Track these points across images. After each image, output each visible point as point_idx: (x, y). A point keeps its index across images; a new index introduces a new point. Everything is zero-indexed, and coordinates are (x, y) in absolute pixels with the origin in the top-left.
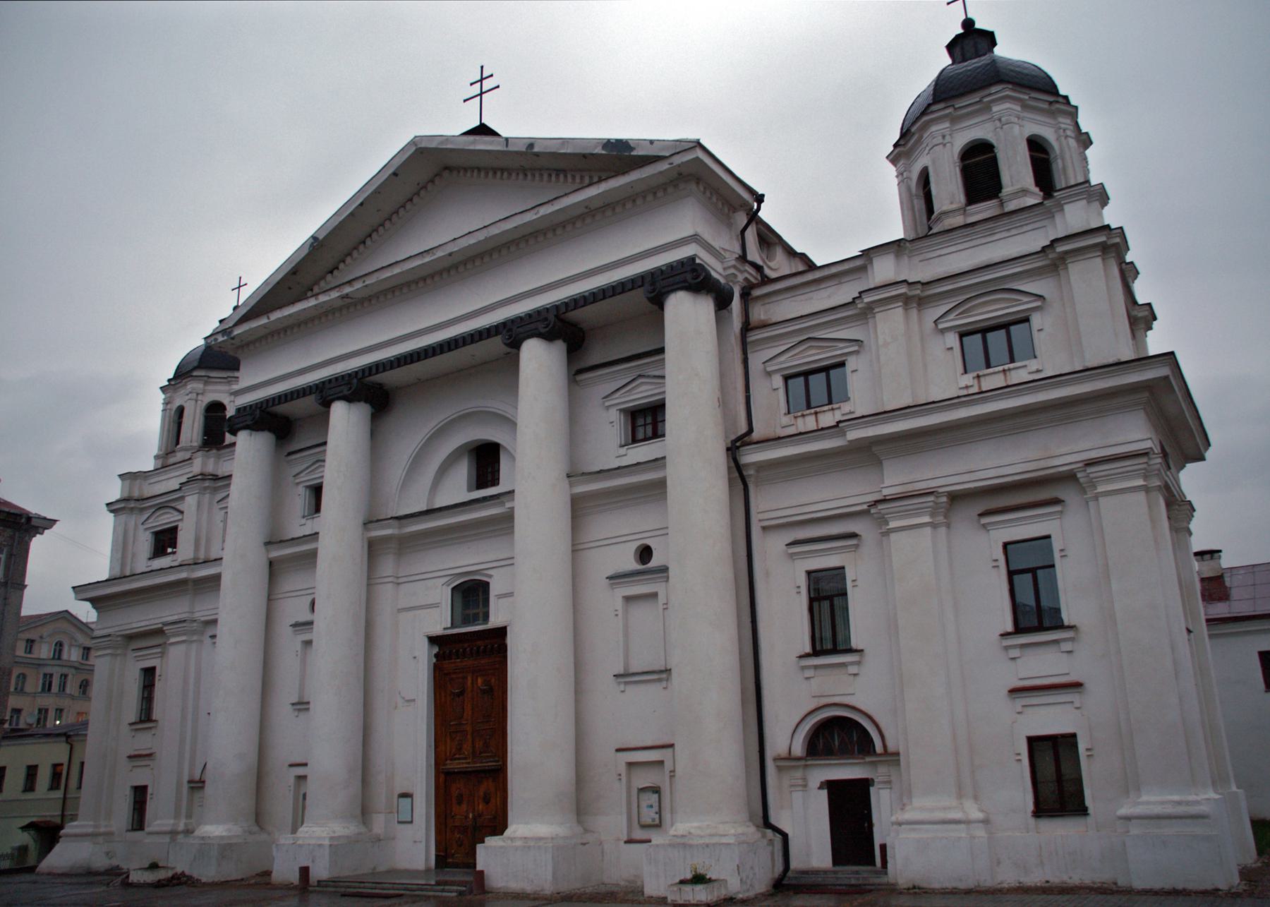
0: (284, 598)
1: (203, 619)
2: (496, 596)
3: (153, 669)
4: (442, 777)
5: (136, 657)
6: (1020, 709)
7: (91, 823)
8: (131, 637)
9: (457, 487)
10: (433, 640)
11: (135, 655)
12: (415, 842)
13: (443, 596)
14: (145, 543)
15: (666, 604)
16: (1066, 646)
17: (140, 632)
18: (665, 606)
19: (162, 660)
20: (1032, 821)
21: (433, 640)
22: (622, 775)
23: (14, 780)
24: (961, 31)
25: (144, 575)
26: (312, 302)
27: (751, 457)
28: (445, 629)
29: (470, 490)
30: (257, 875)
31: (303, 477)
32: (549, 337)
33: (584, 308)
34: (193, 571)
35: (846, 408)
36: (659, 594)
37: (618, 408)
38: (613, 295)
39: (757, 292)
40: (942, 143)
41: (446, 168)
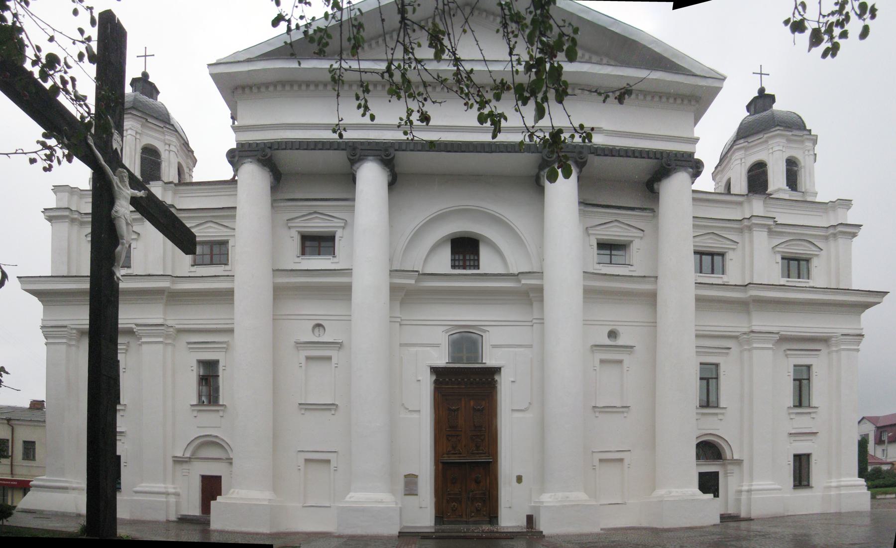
2: (491, 345)
4: (441, 466)
7: (162, 485)
10: (435, 370)
12: (421, 508)
13: (443, 339)
15: (125, 369)
18: (336, 365)
19: (126, 356)
20: (792, 490)
21: (435, 370)
22: (883, 448)
24: (757, 95)
25: (701, 285)
28: (447, 363)
31: (298, 223)
33: (284, 151)
34: (173, 283)
36: (624, 361)
37: (297, 230)
38: (314, 149)
40: (782, 150)
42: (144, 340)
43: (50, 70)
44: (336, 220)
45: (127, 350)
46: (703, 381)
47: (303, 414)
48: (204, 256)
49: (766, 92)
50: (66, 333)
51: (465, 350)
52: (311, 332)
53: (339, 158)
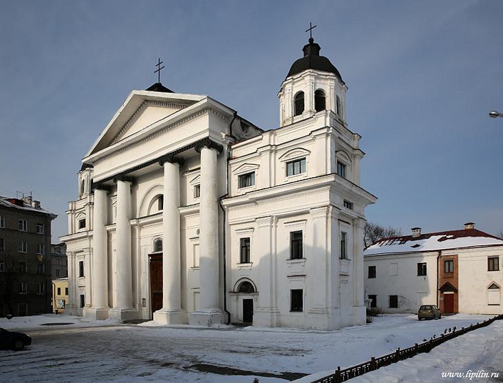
3: (82, 262)
9: (155, 209)
14: (281, 167)
21: (149, 255)
27: (225, 202)
29: (159, 210)
30: (229, 314)
32: (172, 161)
35: (305, 174)
39: (233, 147)
41: (146, 101)
49: (314, 42)
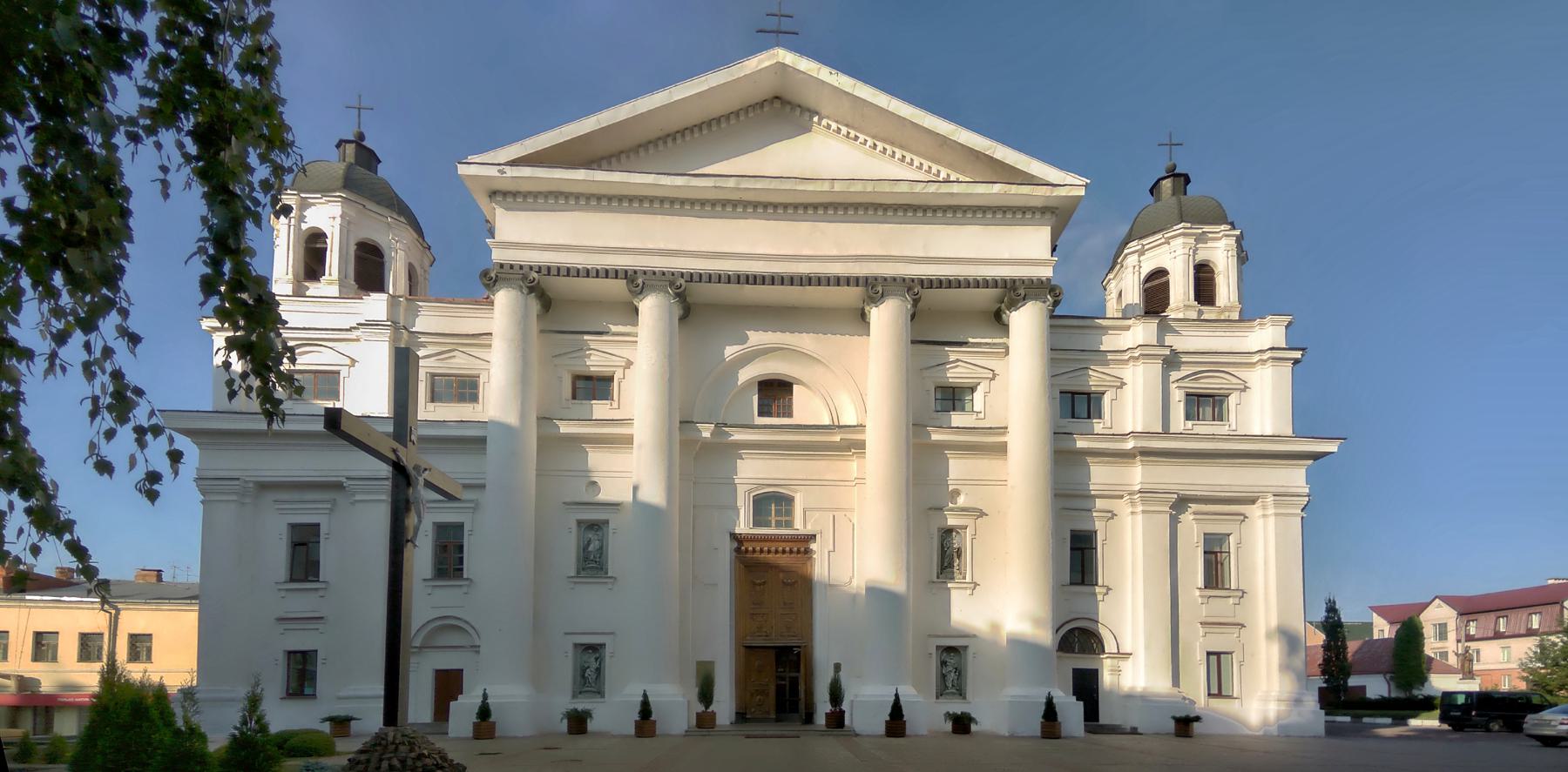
0: (577, 476)
1: (460, 481)
5: (278, 509)
6: (282, 631)
8: (264, 487)
11: (277, 507)
15: (328, 534)
16: (465, 589)
17: (293, 482)
23: (21, 646)
26: (649, 179)
41: (777, 98)
42: (358, 497)
43: (197, 125)
44: (614, 358)
45: (331, 510)
46: (1076, 552)
47: (572, 589)
48: (951, 402)
50: (237, 487)
51: (773, 512)
52: (327, 716)
53: (852, 294)
